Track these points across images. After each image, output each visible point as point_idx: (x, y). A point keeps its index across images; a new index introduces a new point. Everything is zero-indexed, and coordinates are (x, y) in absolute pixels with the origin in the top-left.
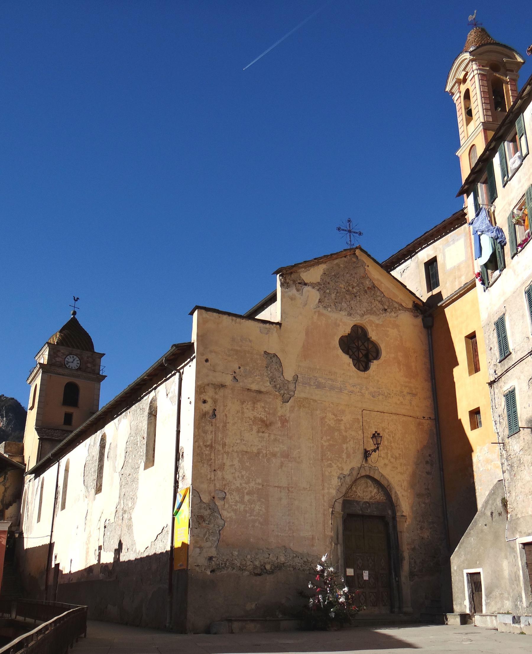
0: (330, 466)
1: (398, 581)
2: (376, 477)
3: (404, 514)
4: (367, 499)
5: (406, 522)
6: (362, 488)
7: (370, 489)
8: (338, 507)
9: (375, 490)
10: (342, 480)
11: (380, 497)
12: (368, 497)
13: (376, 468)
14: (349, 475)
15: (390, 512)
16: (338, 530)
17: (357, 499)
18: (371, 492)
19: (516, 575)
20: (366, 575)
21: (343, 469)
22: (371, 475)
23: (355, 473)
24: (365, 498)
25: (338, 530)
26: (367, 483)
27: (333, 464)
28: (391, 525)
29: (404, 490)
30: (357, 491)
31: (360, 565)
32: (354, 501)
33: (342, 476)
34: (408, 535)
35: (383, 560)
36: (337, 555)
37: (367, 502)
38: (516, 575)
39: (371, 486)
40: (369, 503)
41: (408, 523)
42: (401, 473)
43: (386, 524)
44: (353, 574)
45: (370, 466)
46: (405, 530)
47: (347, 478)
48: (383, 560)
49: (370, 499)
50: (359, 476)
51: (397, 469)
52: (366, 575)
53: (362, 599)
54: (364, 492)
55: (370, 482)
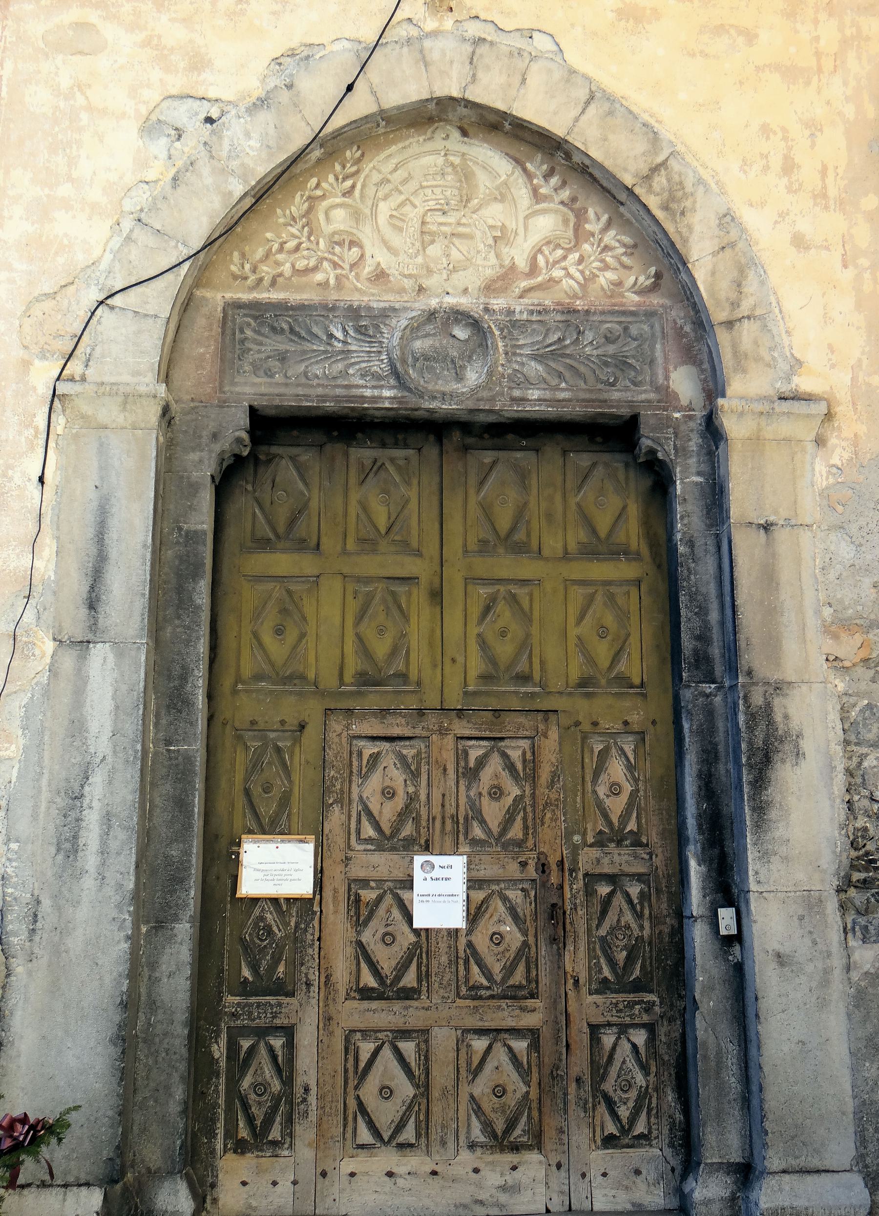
0: (81, 41)
1: (729, 941)
2: (533, 108)
3: (804, 383)
4: (459, 291)
5: (820, 441)
6: (413, 214)
7: (495, 213)
8: (129, 350)
9: (547, 224)
10: (189, 146)
11: (598, 270)
12: (471, 279)
13: (542, 43)
14: (262, 103)
15: (684, 384)
16: (100, 537)
17: (361, 293)
18: (501, 237)
19: (685, 292)
20: (440, 892)
21: (198, 63)
22: (490, 91)
23: (319, 90)
24: (432, 282)
25: (100, 537)
26: (466, 176)
27: (110, 31)
28: (687, 480)
29: (821, 196)
30: (366, 235)
31: (387, 813)
32: (329, 309)
33: (185, 114)
34: (845, 552)
35: (617, 770)
36: (77, 728)
37: (458, 316)
38: (685, 292)
39: (501, 195)
40: (475, 324)
41: (839, 452)
42: (790, 73)
43: (658, 479)
44: (304, 887)
45: (473, 29)
46: (810, 509)
47: (235, 128)
48: (617, 770)
49: (489, 288)
50: (360, 105)
51: (750, 37)
52: (440, 892)
53: (386, 1092)
54: (426, 236)
55: (491, 161)
